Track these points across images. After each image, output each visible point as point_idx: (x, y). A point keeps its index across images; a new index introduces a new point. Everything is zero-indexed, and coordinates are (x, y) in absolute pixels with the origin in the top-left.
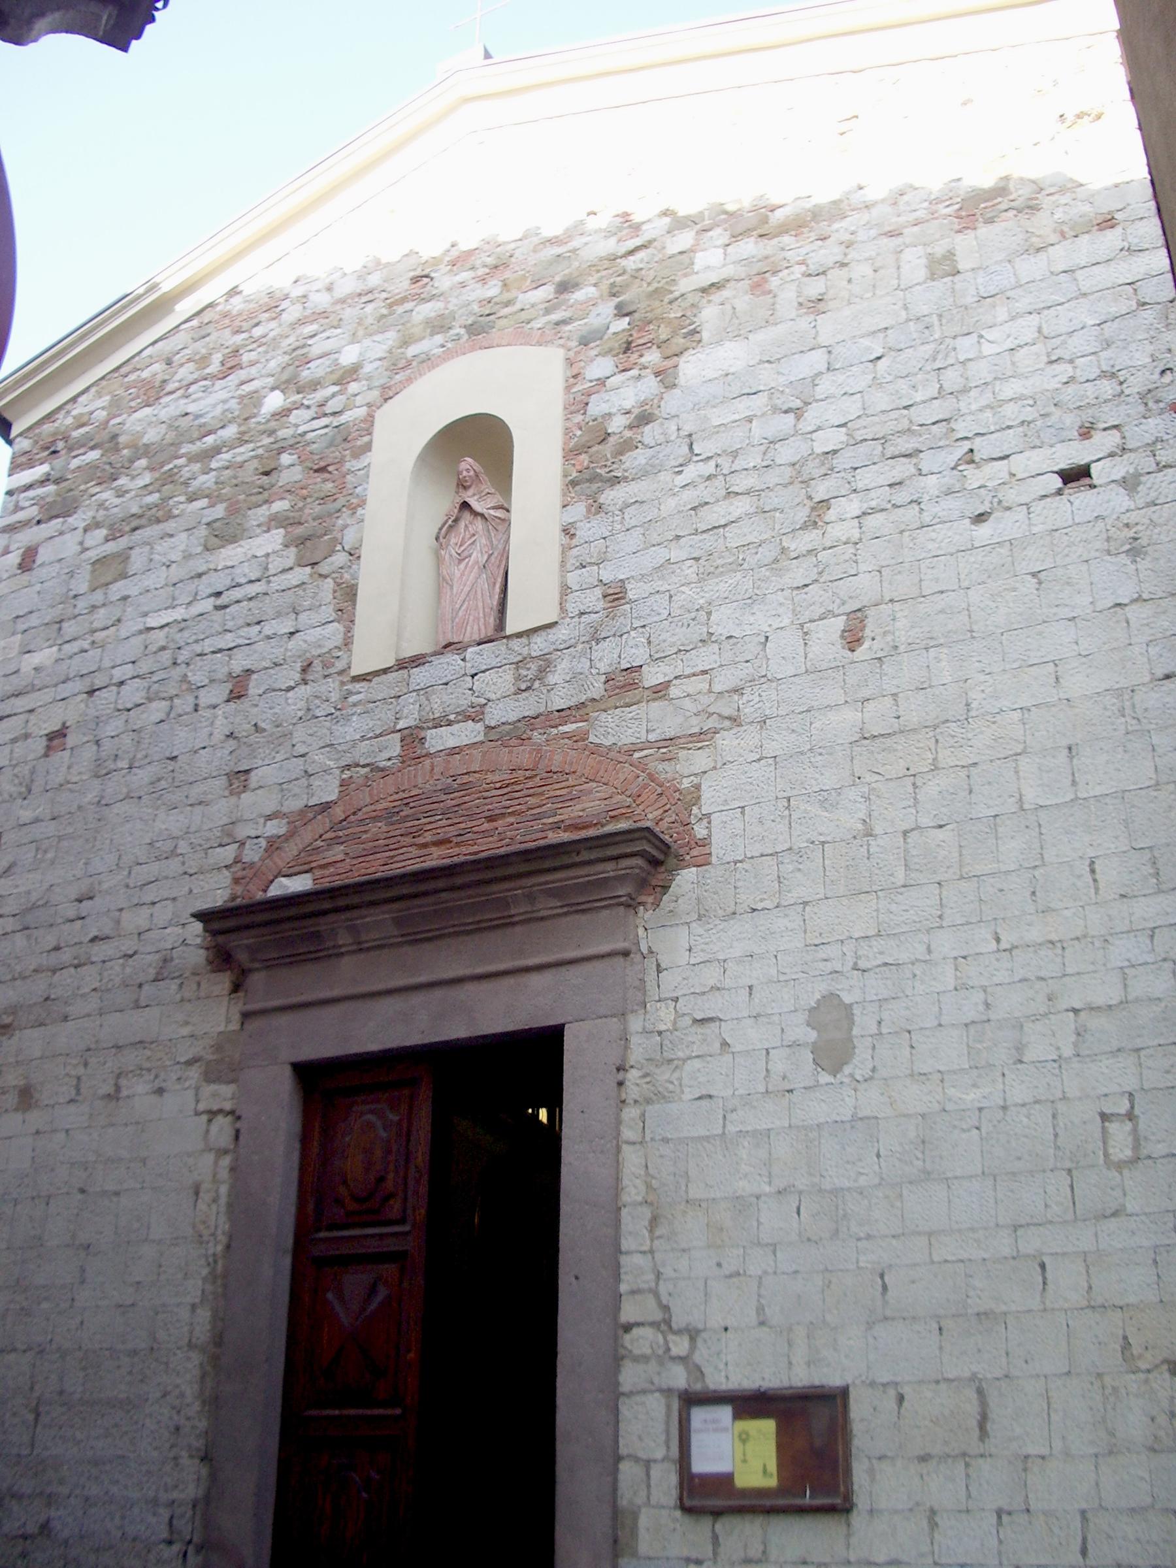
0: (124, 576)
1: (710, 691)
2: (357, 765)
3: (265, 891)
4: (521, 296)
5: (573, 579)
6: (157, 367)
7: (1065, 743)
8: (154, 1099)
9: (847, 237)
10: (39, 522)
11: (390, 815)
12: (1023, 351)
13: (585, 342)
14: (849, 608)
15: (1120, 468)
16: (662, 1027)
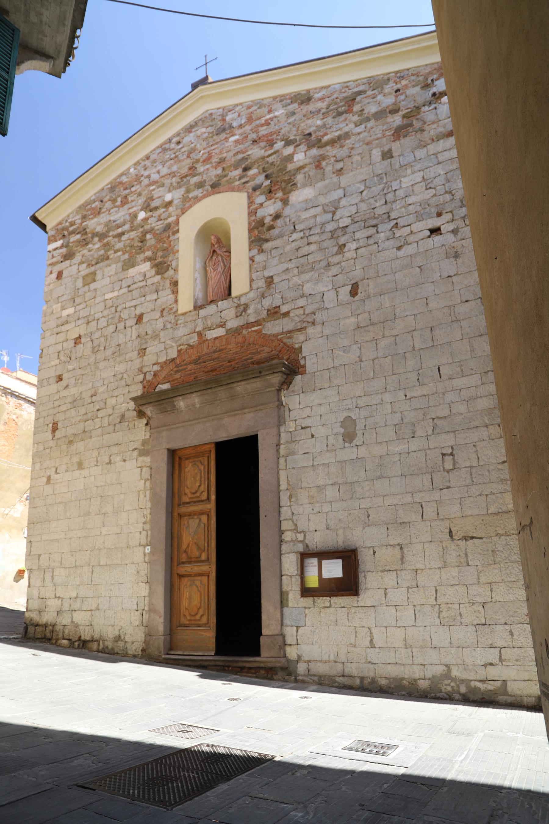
0: (94, 281)
1: (304, 314)
2: (183, 345)
3: (154, 390)
4: (230, 173)
5: (254, 276)
6: (97, 203)
7: (430, 325)
8: (123, 463)
9: (351, 146)
10: (62, 262)
11: (195, 362)
12: (416, 185)
13: (255, 189)
14: (353, 282)
15: (451, 227)
16: (291, 430)
